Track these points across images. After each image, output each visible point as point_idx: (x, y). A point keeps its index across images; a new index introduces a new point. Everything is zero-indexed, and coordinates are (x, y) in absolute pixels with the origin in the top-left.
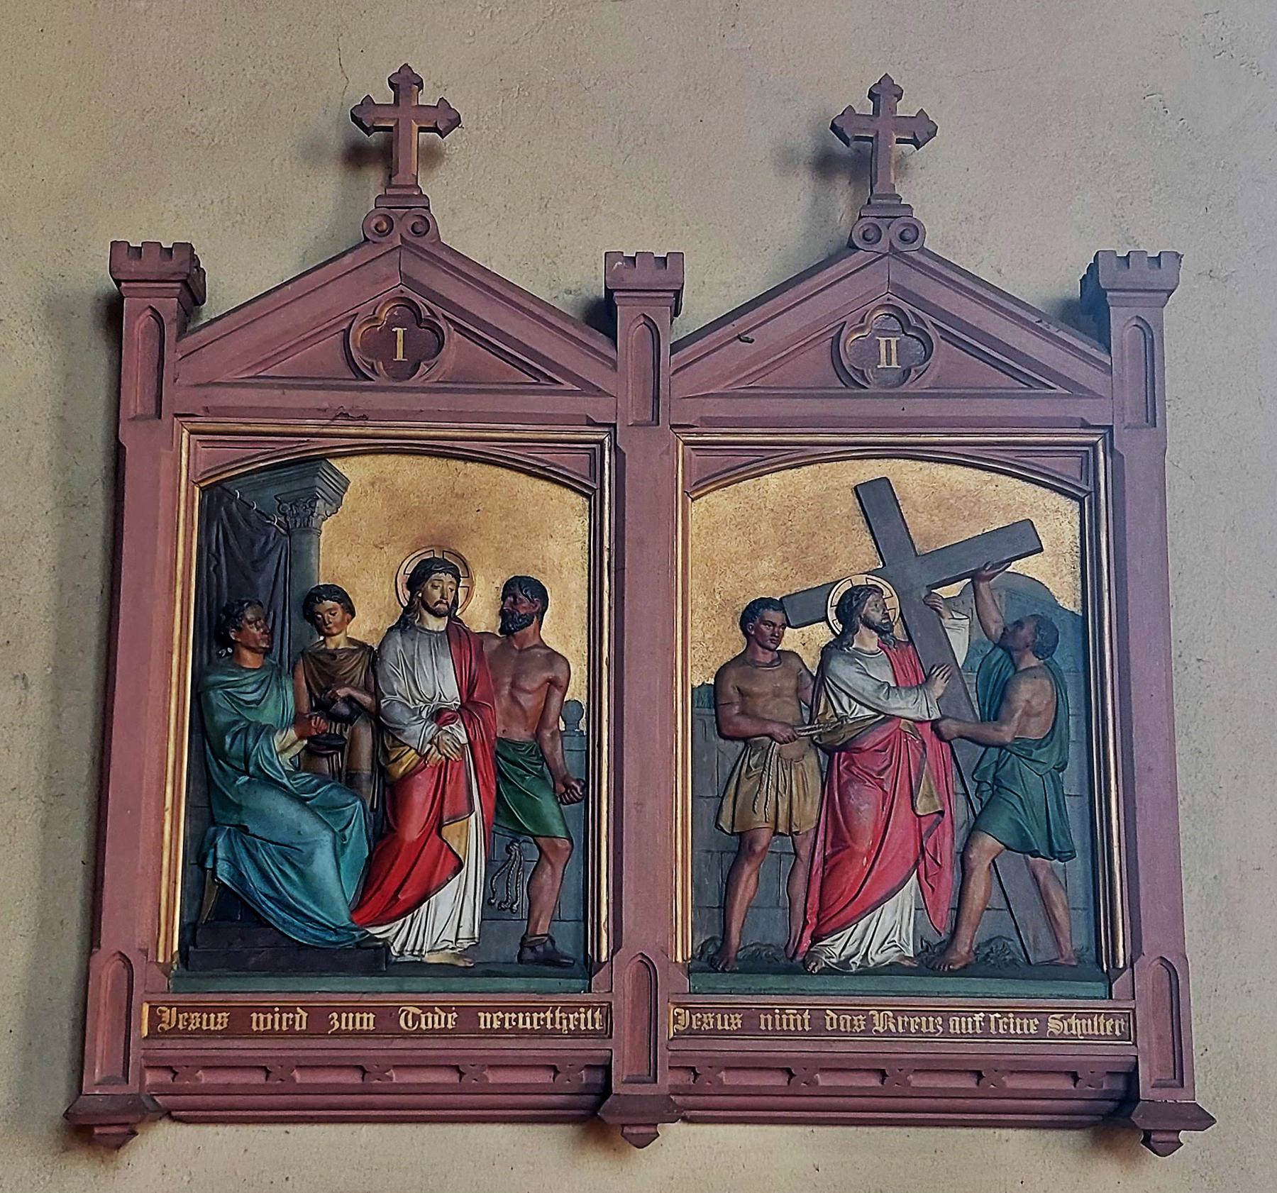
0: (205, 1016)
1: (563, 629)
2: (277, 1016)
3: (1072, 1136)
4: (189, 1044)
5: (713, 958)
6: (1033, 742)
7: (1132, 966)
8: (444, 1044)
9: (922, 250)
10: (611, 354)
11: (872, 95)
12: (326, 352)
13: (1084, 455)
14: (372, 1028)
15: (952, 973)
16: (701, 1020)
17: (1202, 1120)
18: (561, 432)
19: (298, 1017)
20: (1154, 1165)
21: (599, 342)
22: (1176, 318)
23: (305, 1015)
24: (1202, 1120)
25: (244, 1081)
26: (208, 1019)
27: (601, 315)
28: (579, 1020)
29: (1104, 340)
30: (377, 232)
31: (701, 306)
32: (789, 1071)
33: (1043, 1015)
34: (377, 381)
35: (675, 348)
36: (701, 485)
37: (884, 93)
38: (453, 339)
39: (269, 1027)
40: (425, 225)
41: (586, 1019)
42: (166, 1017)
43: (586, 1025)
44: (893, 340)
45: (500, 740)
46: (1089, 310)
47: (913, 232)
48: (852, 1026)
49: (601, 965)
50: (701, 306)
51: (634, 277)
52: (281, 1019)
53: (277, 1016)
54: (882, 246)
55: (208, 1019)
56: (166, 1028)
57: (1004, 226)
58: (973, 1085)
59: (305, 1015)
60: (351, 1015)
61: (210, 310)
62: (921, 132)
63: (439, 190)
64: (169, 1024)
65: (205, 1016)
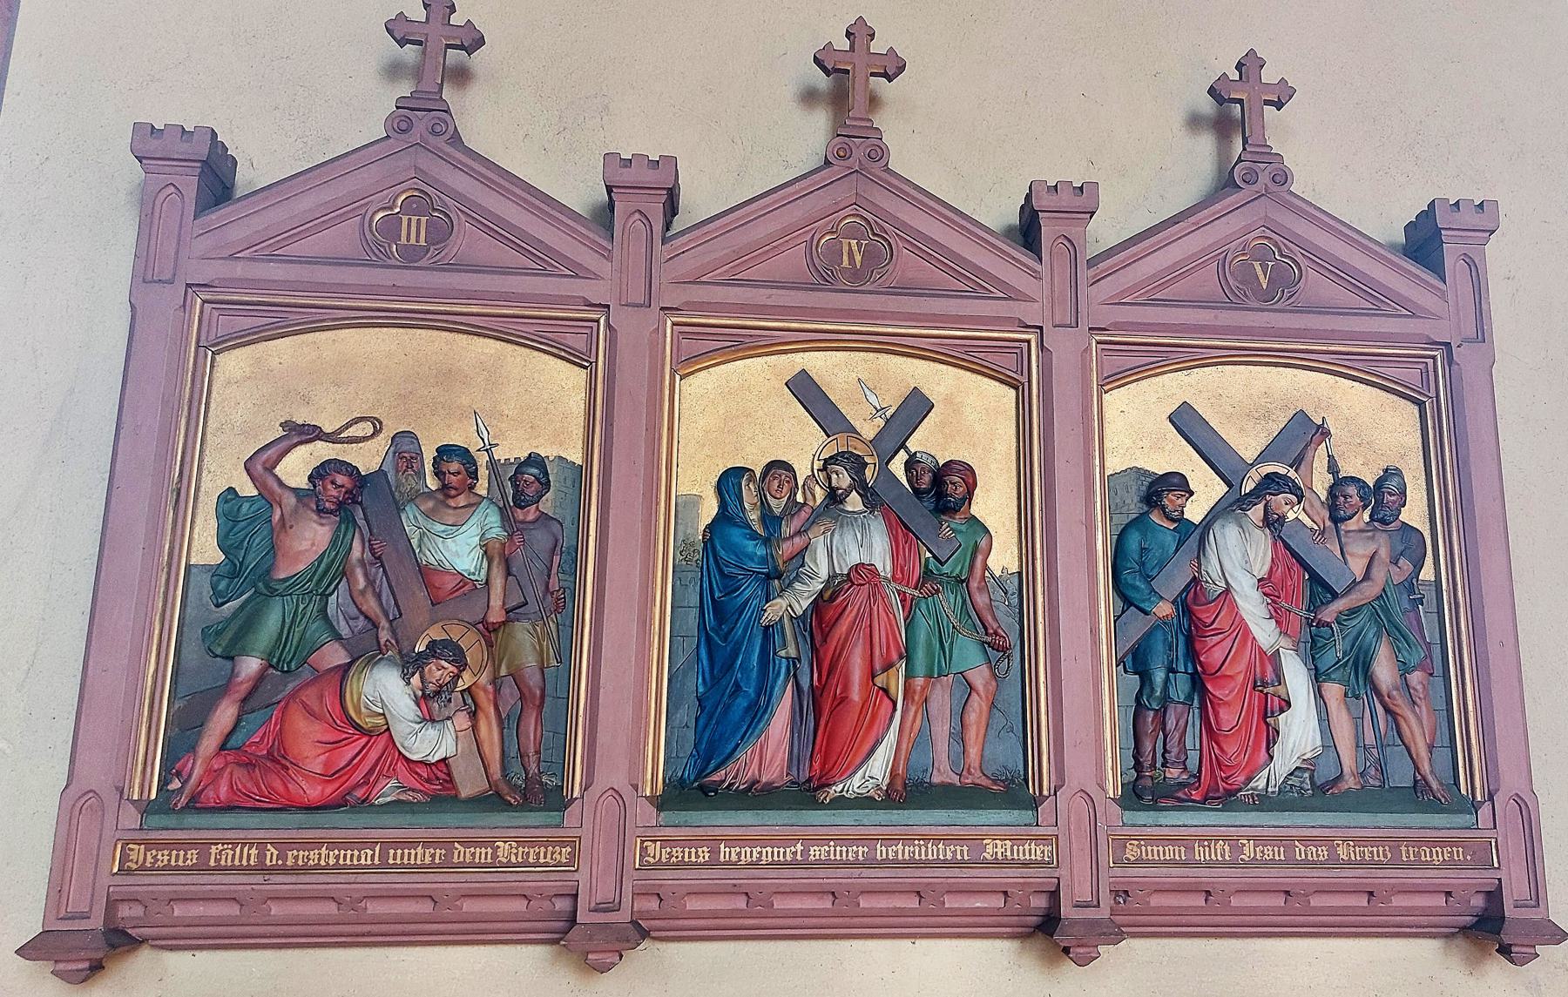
1: (993, 503)
4: (786, 873)
5: (1137, 795)
6: (1386, 600)
7: (1491, 798)
8: (293, 879)
9: (888, 171)
10: (1037, 267)
11: (848, 34)
12: (1206, 282)
13: (1430, 361)
15: (1263, 802)
20: (1497, 970)
21: (1026, 258)
22: (1496, 253)
25: (314, 912)
27: (605, 216)
29: (1438, 269)
30: (1226, 183)
31: (1104, 231)
32: (1005, 893)
33: (448, 844)
34: (393, 262)
35: (1091, 263)
36: (688, 363)
37: (859, 33)
38: (904, 254)
40: (879, 153)
42: (651, 851)
44: (424, 219)
46: (1424, 242)
47: (1282, 178)
48: (697, 856)
49: (573, 800)
50: (1104, 231)
51: (626, 176)
54: (1259, 186)
57: (1349, 176)
58: (829, 905)
61: (679, 224)
62: (892, 68)
63: (893, 129)
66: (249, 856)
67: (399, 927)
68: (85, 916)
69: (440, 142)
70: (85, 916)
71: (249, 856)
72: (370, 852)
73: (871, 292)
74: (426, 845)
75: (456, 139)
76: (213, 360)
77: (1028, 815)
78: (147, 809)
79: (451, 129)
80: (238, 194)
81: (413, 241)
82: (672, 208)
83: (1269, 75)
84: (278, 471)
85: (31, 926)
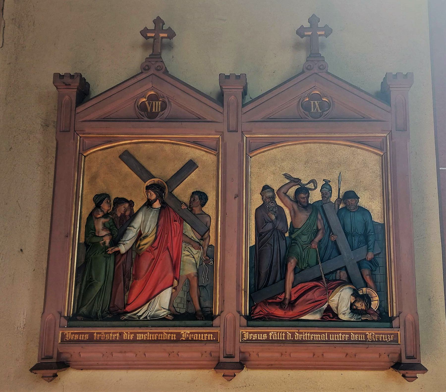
0: (259, 335)
2: (129, 335)
3: (382, 374)
14: (175, 339)
16: (252, 336)
17: (424, 370)
18: (309, 133)
19: (164, 335)
23: (290, 335)
24: (424, 370)
26: (260, 336)
27: (220, 98)
28: (147, 336)
29: (223, 106)
39: (142, 338)
41: (305, 336)
43: (305, 338)
45: (200, 249)
46: (384, 95)
49: (216, 317)
52: (130, 336)
53: (129, 335)
55: (260, 336)
56: (68, 339)
59: (290, 335)
60: (153, 335)
61: (248, 99)
64: (68, 338)
65: (259, 335)
66: (282, 336)
67: (157, 363)
68: (51, 358)
69: (160, 74)
70: (51, 358)
71: (282, 336)
72: (324, 335)
73: (322, 121)
74: (343, 334)
75: (166, 72)
76: (379, 155)
77: (388, 324)
78: (69, 319)
79: (164, 68)
80: (93, 95)
81: (154, 110)
82: (245, 93)
83: (151, 26)
84: (287, 194)
85: (35, 361)
